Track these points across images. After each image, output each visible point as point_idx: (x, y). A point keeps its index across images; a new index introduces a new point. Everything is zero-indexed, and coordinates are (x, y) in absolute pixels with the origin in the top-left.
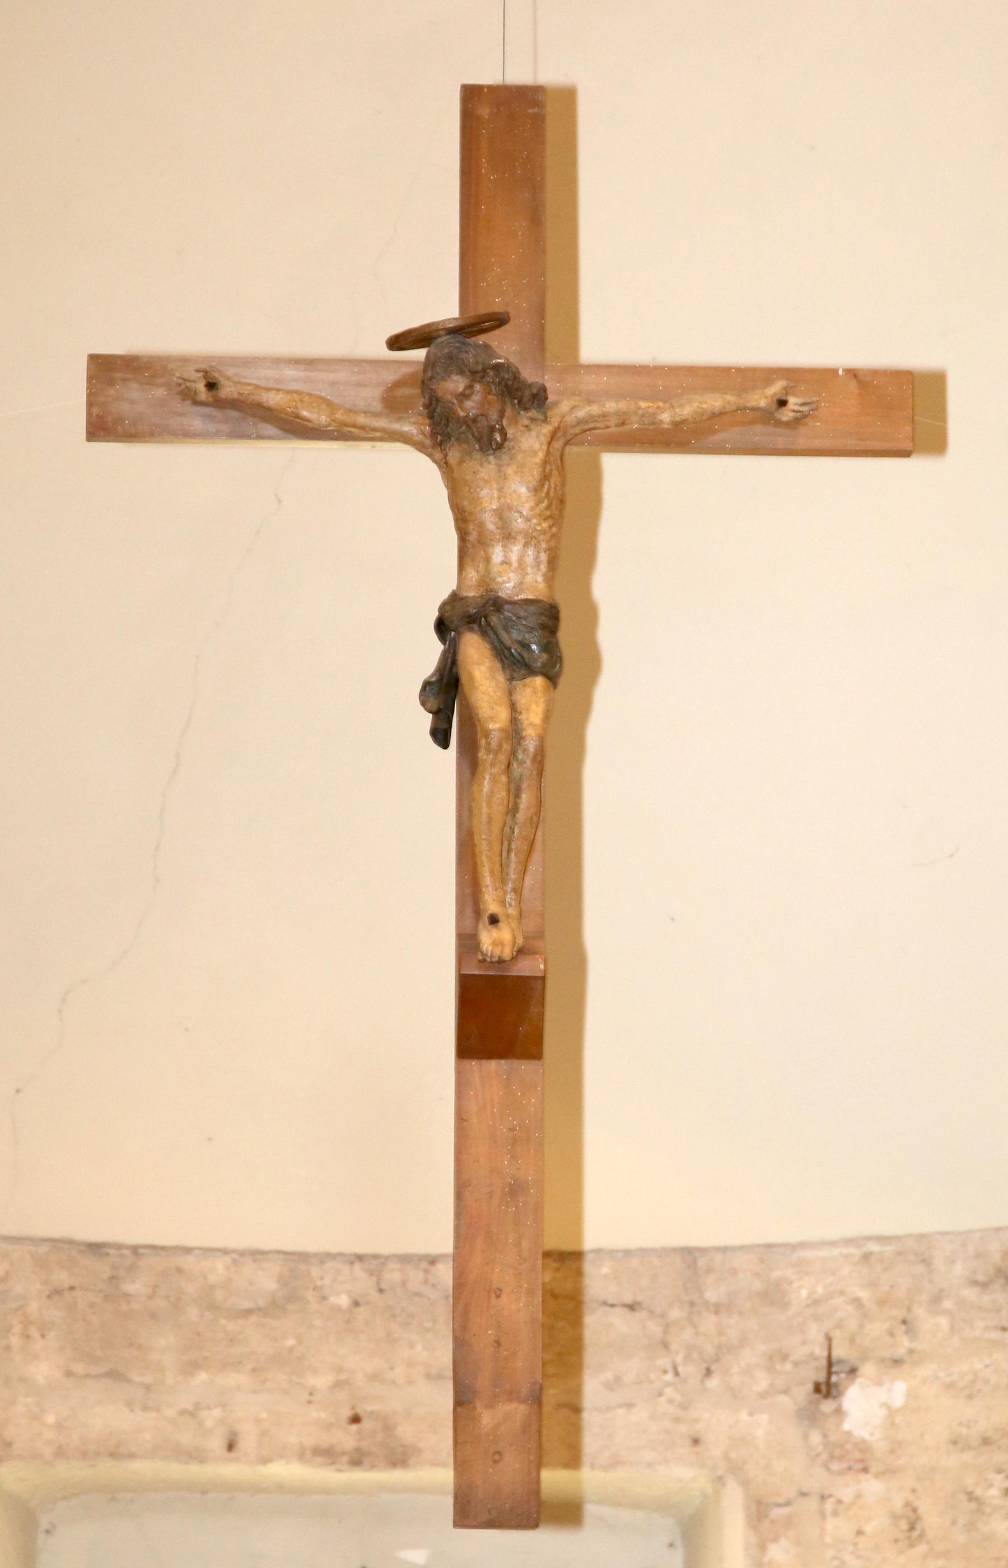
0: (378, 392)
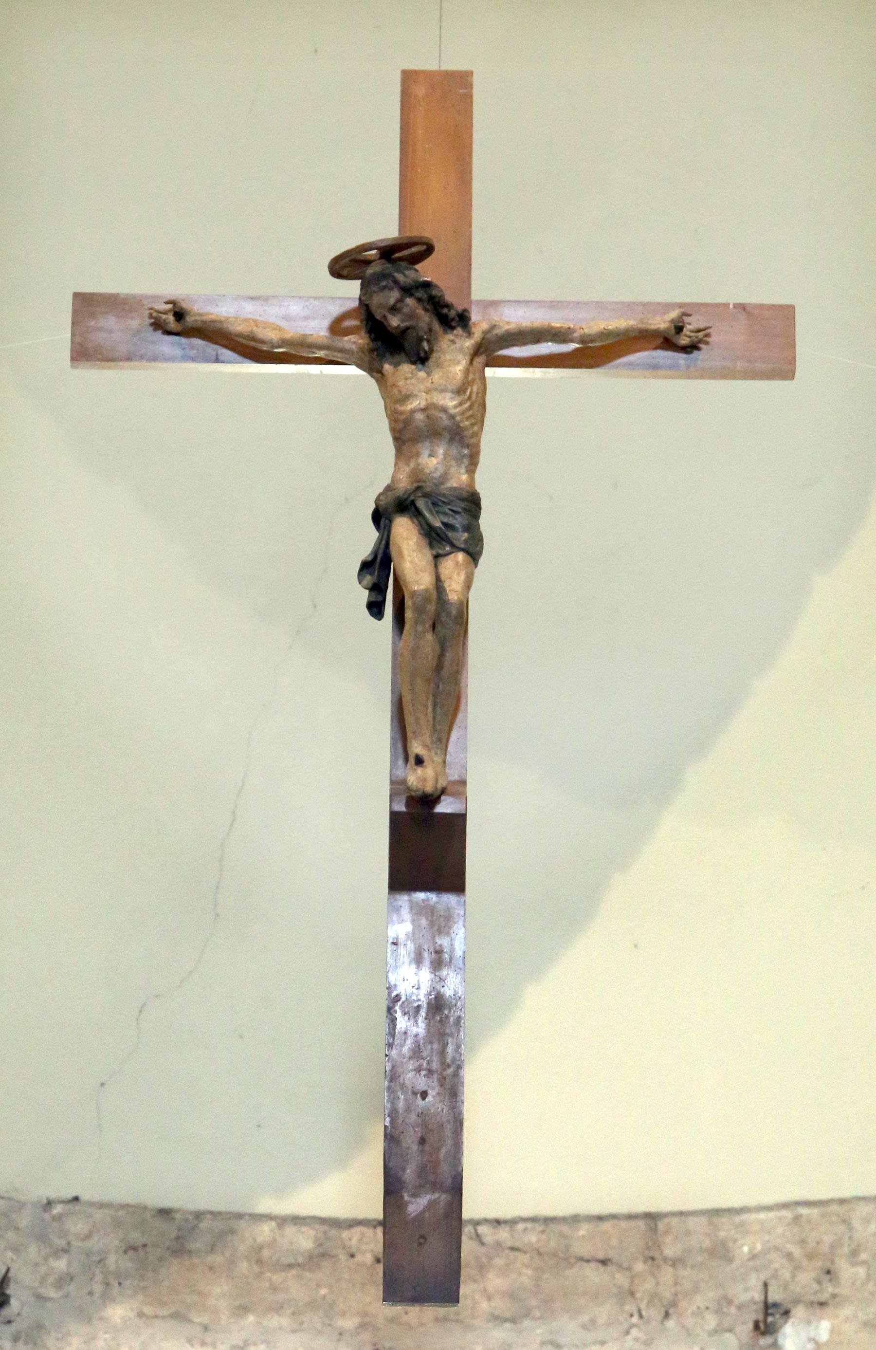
0: (326, 323)
